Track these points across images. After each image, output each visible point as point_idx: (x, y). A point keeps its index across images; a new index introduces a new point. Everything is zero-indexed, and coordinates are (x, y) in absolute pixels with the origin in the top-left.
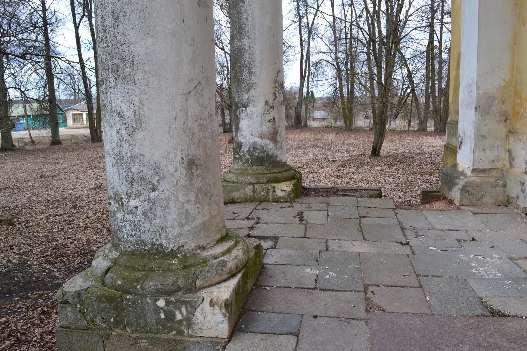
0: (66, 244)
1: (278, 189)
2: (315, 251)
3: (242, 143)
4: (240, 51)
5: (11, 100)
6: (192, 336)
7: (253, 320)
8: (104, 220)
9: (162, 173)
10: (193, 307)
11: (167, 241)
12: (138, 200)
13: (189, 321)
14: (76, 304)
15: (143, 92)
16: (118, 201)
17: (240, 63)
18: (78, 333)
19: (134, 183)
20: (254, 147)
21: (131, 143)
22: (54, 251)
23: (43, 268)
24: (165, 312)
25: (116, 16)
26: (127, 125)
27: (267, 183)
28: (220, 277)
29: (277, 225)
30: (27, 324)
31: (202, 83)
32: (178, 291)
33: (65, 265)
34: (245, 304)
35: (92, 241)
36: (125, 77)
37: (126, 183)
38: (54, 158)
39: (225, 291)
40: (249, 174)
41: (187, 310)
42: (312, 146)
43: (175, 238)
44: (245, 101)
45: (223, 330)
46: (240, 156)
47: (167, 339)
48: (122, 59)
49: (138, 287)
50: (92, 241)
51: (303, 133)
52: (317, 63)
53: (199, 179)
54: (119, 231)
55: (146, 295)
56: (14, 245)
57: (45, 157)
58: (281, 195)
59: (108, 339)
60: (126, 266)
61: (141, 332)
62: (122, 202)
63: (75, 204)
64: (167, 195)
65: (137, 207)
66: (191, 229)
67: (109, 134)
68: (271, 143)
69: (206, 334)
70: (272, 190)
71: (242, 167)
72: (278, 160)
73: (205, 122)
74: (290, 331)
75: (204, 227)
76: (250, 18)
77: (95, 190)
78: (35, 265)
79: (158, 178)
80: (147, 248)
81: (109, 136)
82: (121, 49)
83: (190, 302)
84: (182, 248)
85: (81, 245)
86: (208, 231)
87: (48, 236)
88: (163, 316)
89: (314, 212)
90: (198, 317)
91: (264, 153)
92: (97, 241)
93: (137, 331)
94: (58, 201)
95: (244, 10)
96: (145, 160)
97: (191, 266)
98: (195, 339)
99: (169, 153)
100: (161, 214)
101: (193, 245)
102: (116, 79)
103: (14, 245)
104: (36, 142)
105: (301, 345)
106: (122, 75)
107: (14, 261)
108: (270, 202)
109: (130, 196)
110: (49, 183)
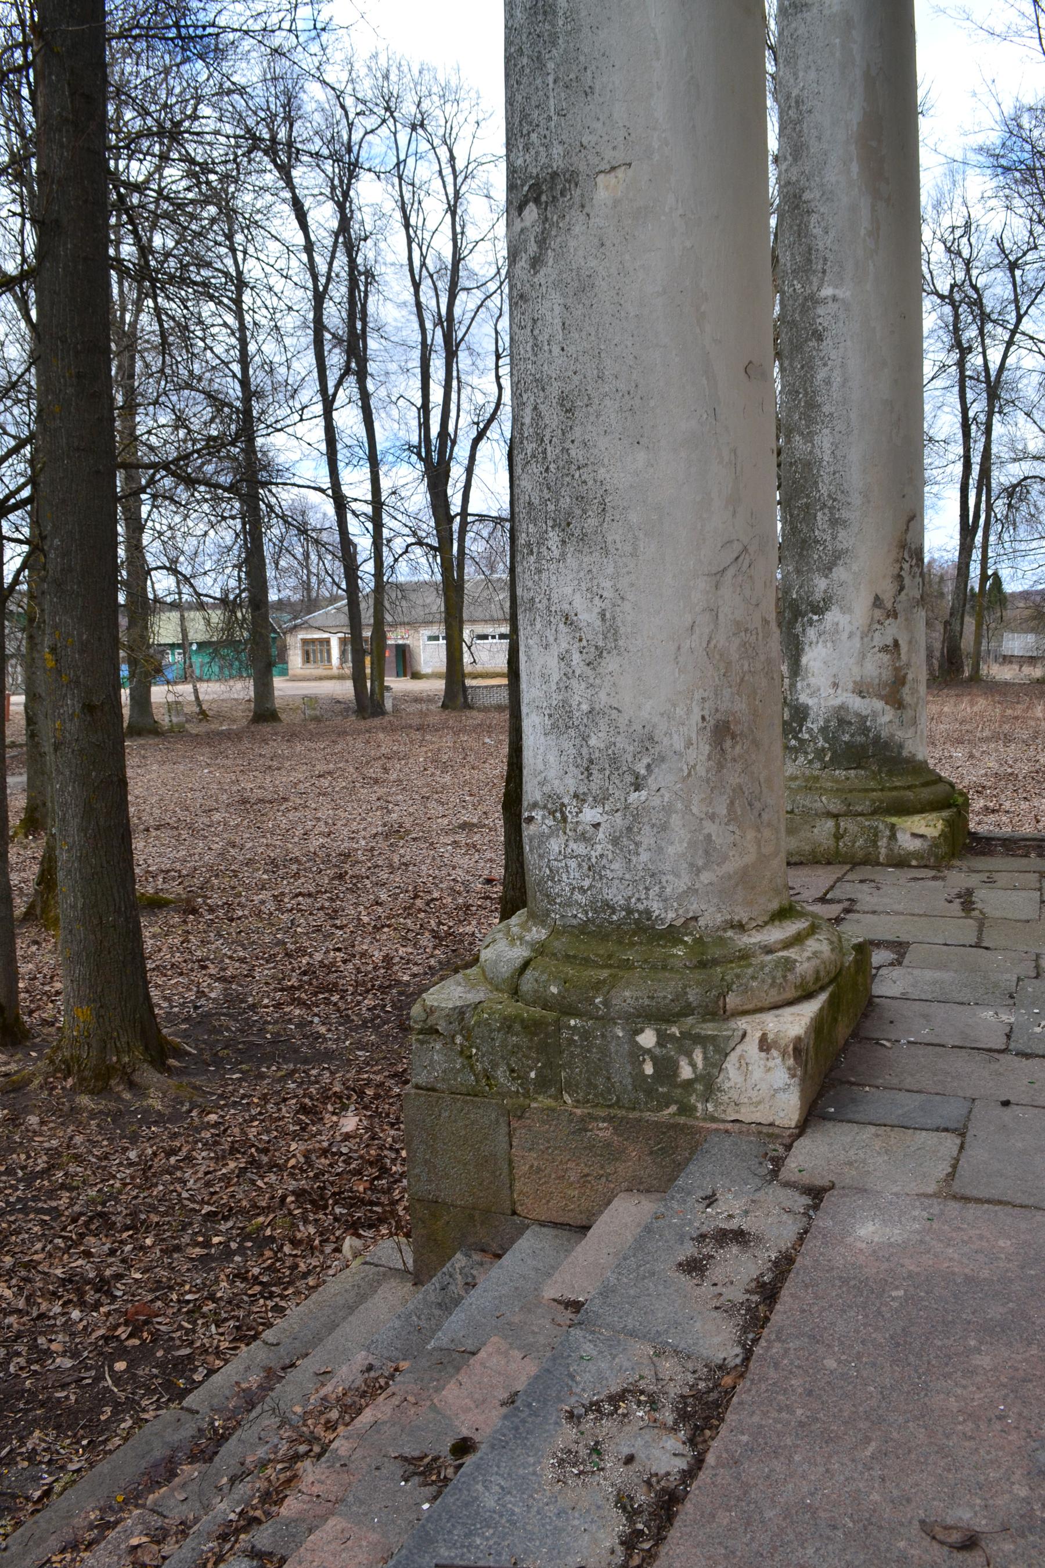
0: (333, 964)
1: (904, 830)
2: (1007, 976)
4: (808, 465)
5: (156, 600)
7: (853, 1101)
8: (420, 910)
9: (658, 748)
10: (719, 1051)
13: (708, 1083)
14: (453, 1037)
16: (552, 813)
17: (808, 496)
18: (455, 1101)
19: (595, 772)
20: (841, 718)
21: (591, 681)
22: (305, 978)
23: (285, 1014)
24: (655, 1059)
25: (568, 406)
26: (584, 643)
27: (874, 813)
28: (779, 993)
29: (902, 917)
30: (268, 1132)
31: (751, 549)
32: (686, 1015)
33: (338, 1010)
34: (831, 1070)
35: (397, 959)
36: (583, 538)
37: (576, 771)
39: (795, 1022)
40: (823, 791)
41: (705, 1058)
42: (995, 737)
43: (680, 898)
44: (818, 596)
46: (802, 741)
47: (656, 1122)
48: (580, 498)
49: (597, 1001)
50: (397, 959)
51: (966, 699)
52: (1014, 486)
53: (739, 767)
54: (553, 880)
55: (613, 1019)
56: (208, 959)
57: (242, 754)
58: (912, 848)
59: (520, 1118)
60: (568, 956)
61: (596, 1105)
62: (563, 813)
63: (343, 871)
64: (666, 799)
65: (599, 824)
66: (715, 879)
68: (888, 707)
69: (747, 1114)
70: (888, 833)
71: (807, 772)
72: (905, 753)
74: (943, 1126)
75: (744, 878)
76: (837, 379)
77: (387, 837)
79: (649, 760)
80: (615, 918)
81: (538, 668)
82: (577, 476)
83: (714, 1038)
84: (693, 923)
85: (370, 968)
86: (753, 888)
87: (285, 943)
88: (649, 1069)
89: (1001, 892)
91: (867, 736)
92: (408, 962)
93: (588, 1101)
94: (296, 860)
95: (822, 359)
96: (621, 720)
97: (715, 962)
98: (721, 1126)
99: (674, 706)
100: (652, 841)
101: (719, 918)
102: (564, 542)
103: (208, 959)
105: (968, 1151)
107: (213, 995)
108: (882, 865)
109: (584, 801)
110: (264, 818)
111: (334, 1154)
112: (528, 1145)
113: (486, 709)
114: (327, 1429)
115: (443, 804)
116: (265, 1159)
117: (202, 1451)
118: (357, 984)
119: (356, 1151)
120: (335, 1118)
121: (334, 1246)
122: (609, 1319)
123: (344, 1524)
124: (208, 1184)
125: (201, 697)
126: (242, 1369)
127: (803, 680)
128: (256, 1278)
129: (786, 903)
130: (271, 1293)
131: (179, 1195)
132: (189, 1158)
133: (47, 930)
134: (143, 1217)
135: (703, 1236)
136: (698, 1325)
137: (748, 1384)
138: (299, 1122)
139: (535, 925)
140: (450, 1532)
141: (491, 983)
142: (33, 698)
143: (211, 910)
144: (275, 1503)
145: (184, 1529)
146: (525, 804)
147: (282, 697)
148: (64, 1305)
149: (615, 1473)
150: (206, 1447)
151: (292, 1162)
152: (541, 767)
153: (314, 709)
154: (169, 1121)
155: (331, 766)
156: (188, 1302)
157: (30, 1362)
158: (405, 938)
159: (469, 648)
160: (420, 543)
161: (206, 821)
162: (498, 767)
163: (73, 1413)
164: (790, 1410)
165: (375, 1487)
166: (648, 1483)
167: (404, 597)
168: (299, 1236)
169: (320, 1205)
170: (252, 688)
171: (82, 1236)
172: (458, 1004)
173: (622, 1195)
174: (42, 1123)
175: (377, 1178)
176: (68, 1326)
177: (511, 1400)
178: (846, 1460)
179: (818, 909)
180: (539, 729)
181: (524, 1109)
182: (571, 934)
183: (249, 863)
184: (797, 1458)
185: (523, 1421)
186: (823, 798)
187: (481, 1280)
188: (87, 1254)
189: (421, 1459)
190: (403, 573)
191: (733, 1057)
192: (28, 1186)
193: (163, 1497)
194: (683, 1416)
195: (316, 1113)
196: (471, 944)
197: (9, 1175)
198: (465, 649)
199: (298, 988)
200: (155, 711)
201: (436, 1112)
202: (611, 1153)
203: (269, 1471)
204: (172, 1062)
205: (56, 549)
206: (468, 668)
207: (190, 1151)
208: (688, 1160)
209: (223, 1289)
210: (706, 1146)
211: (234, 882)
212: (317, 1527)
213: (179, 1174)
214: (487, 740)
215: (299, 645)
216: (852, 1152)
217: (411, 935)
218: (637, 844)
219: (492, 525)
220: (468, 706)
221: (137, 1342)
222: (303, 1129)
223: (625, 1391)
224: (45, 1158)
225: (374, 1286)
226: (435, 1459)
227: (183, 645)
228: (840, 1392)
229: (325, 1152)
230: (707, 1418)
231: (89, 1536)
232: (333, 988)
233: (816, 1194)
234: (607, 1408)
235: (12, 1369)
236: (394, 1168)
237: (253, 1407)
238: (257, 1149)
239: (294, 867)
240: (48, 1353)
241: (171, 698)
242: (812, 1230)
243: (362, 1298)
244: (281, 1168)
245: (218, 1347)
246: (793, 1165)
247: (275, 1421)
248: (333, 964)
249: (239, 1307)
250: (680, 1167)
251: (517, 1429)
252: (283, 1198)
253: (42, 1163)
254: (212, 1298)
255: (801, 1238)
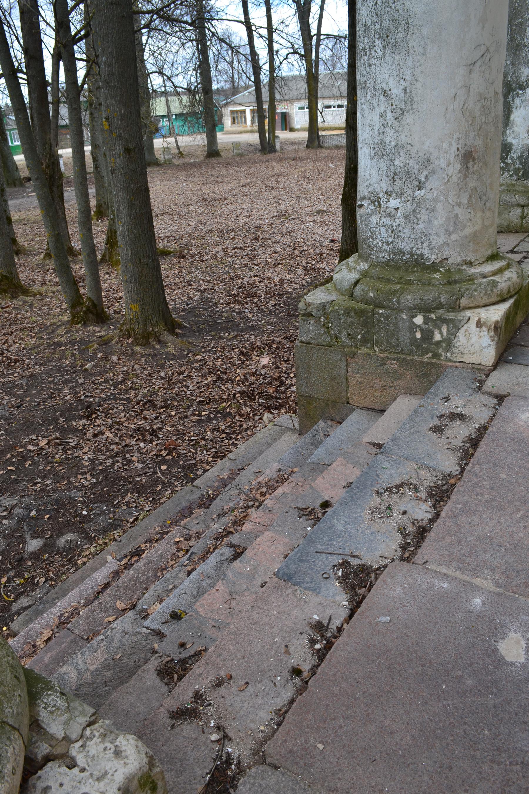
0: (254, 283)
3: (511, 145)
5: (154, 91)
6: (450, 361)
7: (522, 354)
8: (297, 256)
11: (429, 251)
12: (399, 200)
14: (320, 318)
15: (418, 64)
16: (373, 202)
17: (522, 18)
18: (320, 349)
22: (240, 290)
24: (422, 331)
26: (394, 107)
28: (488, 299)
30: (226, 364)
31: (491, 50)
32: (439, 309)
33: (257, 306)
34: (512, 339)
37: (387, 179)
38: (213, 176)
39: (496, 313)
41: (448, 330)
45: (489, 356)
48: (394, 21)
49: (394, 300)
53: (475, 177)
54: (372, 238)
57: (202, 175)
59: (352, 358)
60: (379, 278)
61: (391, 353)
62: (379, 202)
64: (435, 195)
65: (398, 208)
66: (459, 238)
67: (370, 118)
69: (467, 359)
71: (509, 182)
73: (489, 102)
75: (474, 238)
77: (279, 218)
78: (222, 304)
79: (427, 173)
80: (404, 258)
81: (368, 122)
82: (393, 7)
83: (452, 321)
84: (446, 261)
85: (272, 285)
86: (478, 243)
87: (230, 273)
88: (418, 335)
90: (460, 339)
93: (387, 350)
94: (233, 230)
97: (456, 282)
98: (454, 364)
99: (442, 142)
100: (426, 218)
101: (459, 259)
102: (384, 47)
104: (184, 153)
106: (392, 41)
107: (195, 299)
109: (390, 195)
110: (216, 209)
111: (258, 375)
112: (356, 371)
113: (329, 148)
114: (261, 496)
115: (308, 200)
116: (225, 377)
117: (204, 504)
118: (266, 293)
119: (268, 374)
120: (258, 358)
121: (259, 417)
122: (396, 451)
123: (272, 534)
124: (199, 388)
125: (179, 144)
126: (220, 469)
127: (511, 128)
128: (223, 430)
129: (495, 252)
130: (231, 437)
131: (186, 393)
132: (189, 376)
133: (112, 267)
134: (169, 402)
135: (443, 416)
136: (439, 456)
137: (462, 483)
138: (241, 360)
139: (362, 262)
140: (322, 539)
141: (339, 291)
142: (95, 146)
143: (192, 256)
144: (239, 526)
145: (198, 536)
146: (358, 197)
147: (221, 143)
148: (136, 441)
149: (397, 518)
150: (206, 502)
151: (238, 378)
152: (368, 177)
153: (238, 149)
154: (178, 358)
155: (249, 180)
156: (193, 440)
157: (123, 465)
158: (290, 270)
159: (321, 113)
160: (296, 52)
161: (186, 210)
162: (338, 179)
163: (144, 487)
164: (482, 495)
165: (286, 520)
166: (413, 523)
167: (286, 85)
168: (243, 412)
169: (252, 398)
170: (206, 138)
171: (142, 410)
172: (323, 301)
173: (402, 396)
174: (119, 359)
175: (279, 386)
176: (139, 450)
177: (349, 485)
178: (508, 518)
179: (509, 255)
180: (368, 156)
181: (354, 354)
182: (381, 266)
183: (209, 232)
184: (484, 516)
185: (355, 494)
186: (517, 196)
187: (332, 433)
188: (145, 419)
189: (307, 509)
190: (285, 71)
191: (462, 330)
192: (116, 388)
193: (188, 522)
194: (430, 495)
195: (248, 356)
196: (323, 273)
197: (106, 383)
198: (319, 114)
199: (237, 295)
200: (156, 153)
201: (311, 355)
202: (397, 376)
203: (236, 513)
204: (178, 331)
205: (105, 63)
206: (320, 125)
207: (189, 373)
208: (436, 380)
209: (208, 435)
210: (446, 373)
211: (202, 242)
212: (259, 536)
213: (185, 383)
214: (331, 165)
215: (229, 114)
216: (520, 379)
217: (292, 269)
218: (418, 219)
219: (334, 40)
220: (320, 146)
221: (171, 457)
222: (243, 363)
223: (403, 483)
224: (122, 375)
225: (280, 435)
226: (313, 509)
227: (168, 116)
228: (507, 488)
229: (253, 374)
230: (442, 497)
231: (157, 537)
232: (254, 295)
233: (500, 398)
234: (395, 490)
235: (116, 468)
236: (287, 382)
237: (226, 486)
238: (221, 372)
239: (232, 234)
240: (131, 461)
241: (165, 145)
242: (498, 415)
243: (274, 440)
244: (233, 381)
245: (207, 460)
246: (489, 384)
247: (236, 492)
248: (254, 283)
249: (216, 443)
250: (432, 383)
251: (352, 497)
252: (235, 395)
253: (121, 377)
254: (204, 439)
255: (492, 418)
